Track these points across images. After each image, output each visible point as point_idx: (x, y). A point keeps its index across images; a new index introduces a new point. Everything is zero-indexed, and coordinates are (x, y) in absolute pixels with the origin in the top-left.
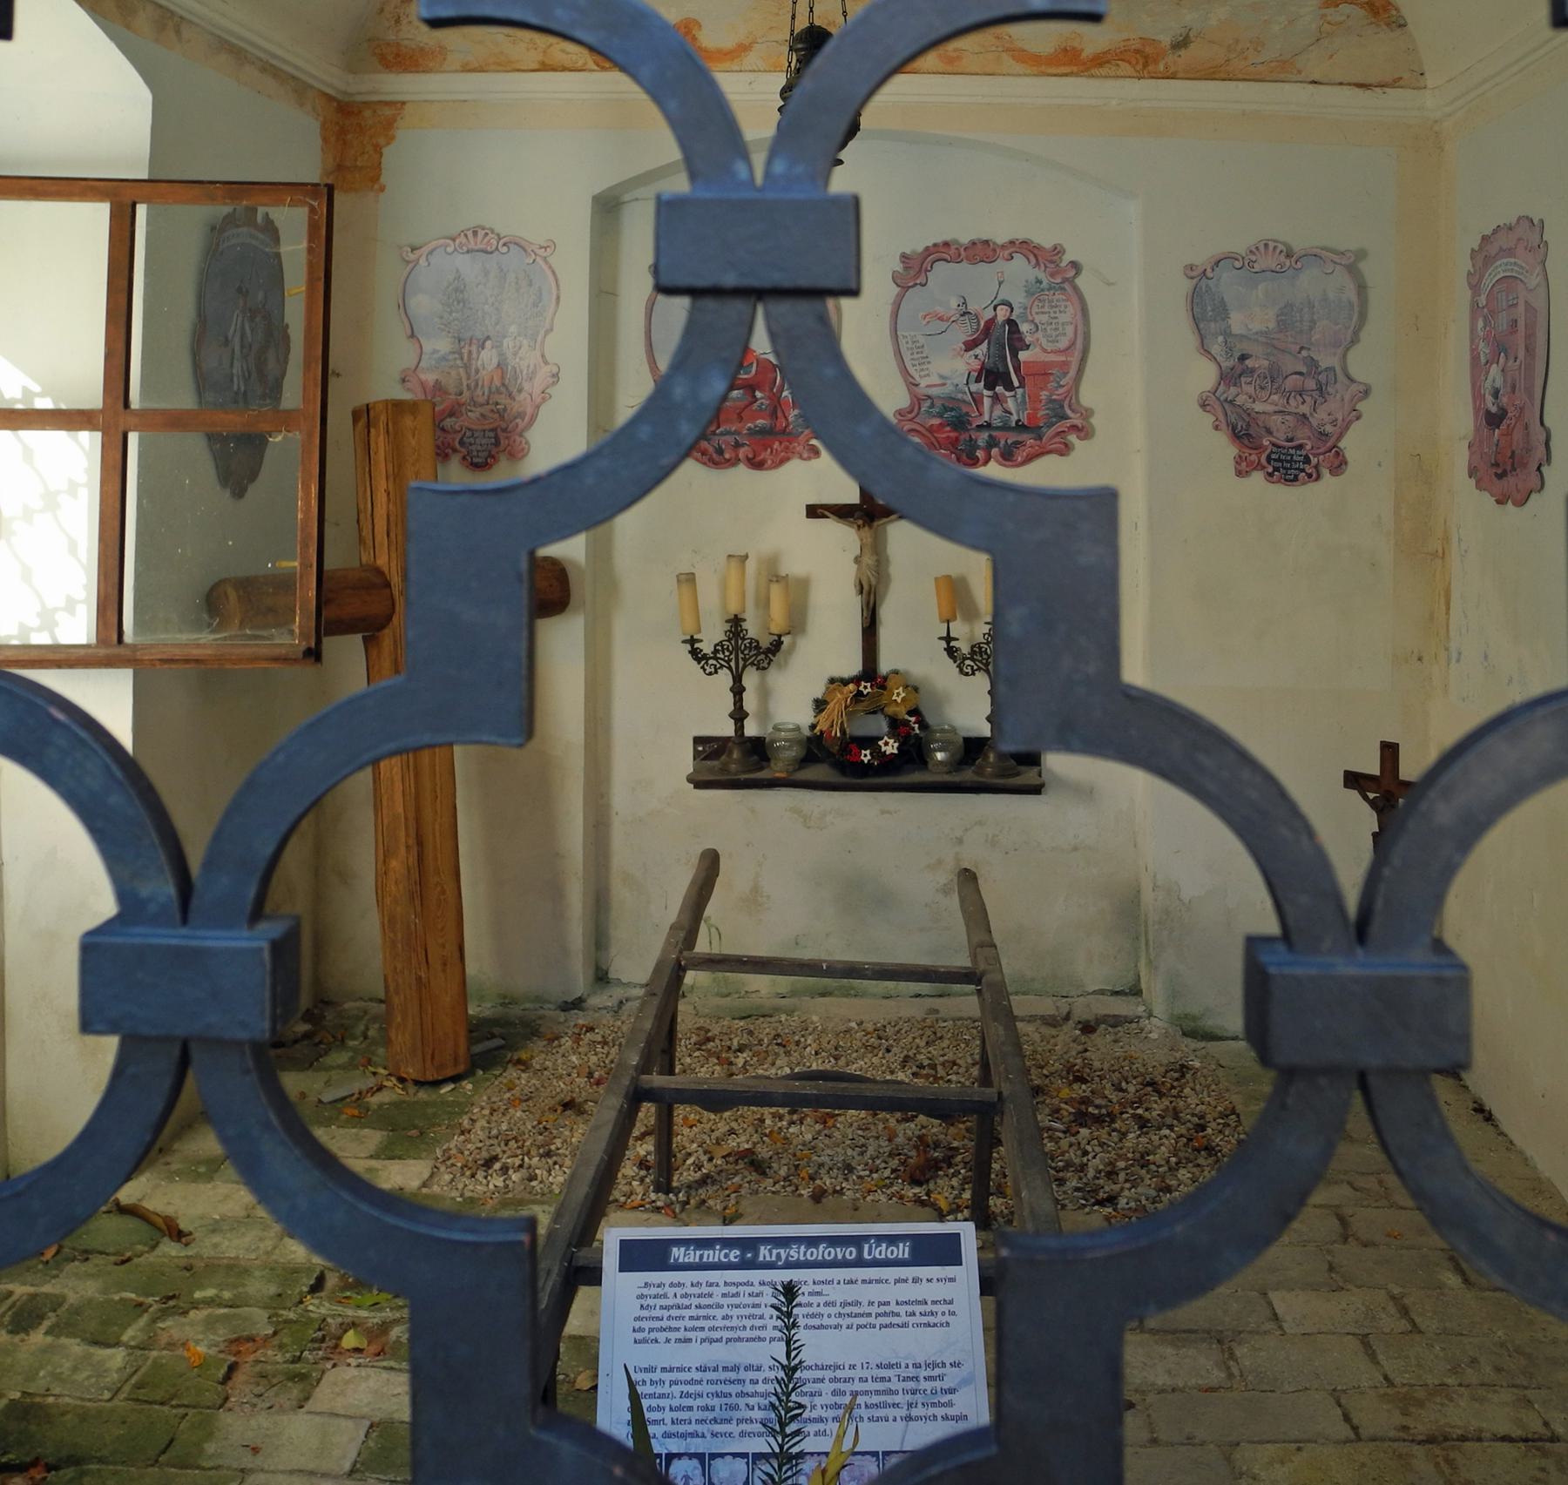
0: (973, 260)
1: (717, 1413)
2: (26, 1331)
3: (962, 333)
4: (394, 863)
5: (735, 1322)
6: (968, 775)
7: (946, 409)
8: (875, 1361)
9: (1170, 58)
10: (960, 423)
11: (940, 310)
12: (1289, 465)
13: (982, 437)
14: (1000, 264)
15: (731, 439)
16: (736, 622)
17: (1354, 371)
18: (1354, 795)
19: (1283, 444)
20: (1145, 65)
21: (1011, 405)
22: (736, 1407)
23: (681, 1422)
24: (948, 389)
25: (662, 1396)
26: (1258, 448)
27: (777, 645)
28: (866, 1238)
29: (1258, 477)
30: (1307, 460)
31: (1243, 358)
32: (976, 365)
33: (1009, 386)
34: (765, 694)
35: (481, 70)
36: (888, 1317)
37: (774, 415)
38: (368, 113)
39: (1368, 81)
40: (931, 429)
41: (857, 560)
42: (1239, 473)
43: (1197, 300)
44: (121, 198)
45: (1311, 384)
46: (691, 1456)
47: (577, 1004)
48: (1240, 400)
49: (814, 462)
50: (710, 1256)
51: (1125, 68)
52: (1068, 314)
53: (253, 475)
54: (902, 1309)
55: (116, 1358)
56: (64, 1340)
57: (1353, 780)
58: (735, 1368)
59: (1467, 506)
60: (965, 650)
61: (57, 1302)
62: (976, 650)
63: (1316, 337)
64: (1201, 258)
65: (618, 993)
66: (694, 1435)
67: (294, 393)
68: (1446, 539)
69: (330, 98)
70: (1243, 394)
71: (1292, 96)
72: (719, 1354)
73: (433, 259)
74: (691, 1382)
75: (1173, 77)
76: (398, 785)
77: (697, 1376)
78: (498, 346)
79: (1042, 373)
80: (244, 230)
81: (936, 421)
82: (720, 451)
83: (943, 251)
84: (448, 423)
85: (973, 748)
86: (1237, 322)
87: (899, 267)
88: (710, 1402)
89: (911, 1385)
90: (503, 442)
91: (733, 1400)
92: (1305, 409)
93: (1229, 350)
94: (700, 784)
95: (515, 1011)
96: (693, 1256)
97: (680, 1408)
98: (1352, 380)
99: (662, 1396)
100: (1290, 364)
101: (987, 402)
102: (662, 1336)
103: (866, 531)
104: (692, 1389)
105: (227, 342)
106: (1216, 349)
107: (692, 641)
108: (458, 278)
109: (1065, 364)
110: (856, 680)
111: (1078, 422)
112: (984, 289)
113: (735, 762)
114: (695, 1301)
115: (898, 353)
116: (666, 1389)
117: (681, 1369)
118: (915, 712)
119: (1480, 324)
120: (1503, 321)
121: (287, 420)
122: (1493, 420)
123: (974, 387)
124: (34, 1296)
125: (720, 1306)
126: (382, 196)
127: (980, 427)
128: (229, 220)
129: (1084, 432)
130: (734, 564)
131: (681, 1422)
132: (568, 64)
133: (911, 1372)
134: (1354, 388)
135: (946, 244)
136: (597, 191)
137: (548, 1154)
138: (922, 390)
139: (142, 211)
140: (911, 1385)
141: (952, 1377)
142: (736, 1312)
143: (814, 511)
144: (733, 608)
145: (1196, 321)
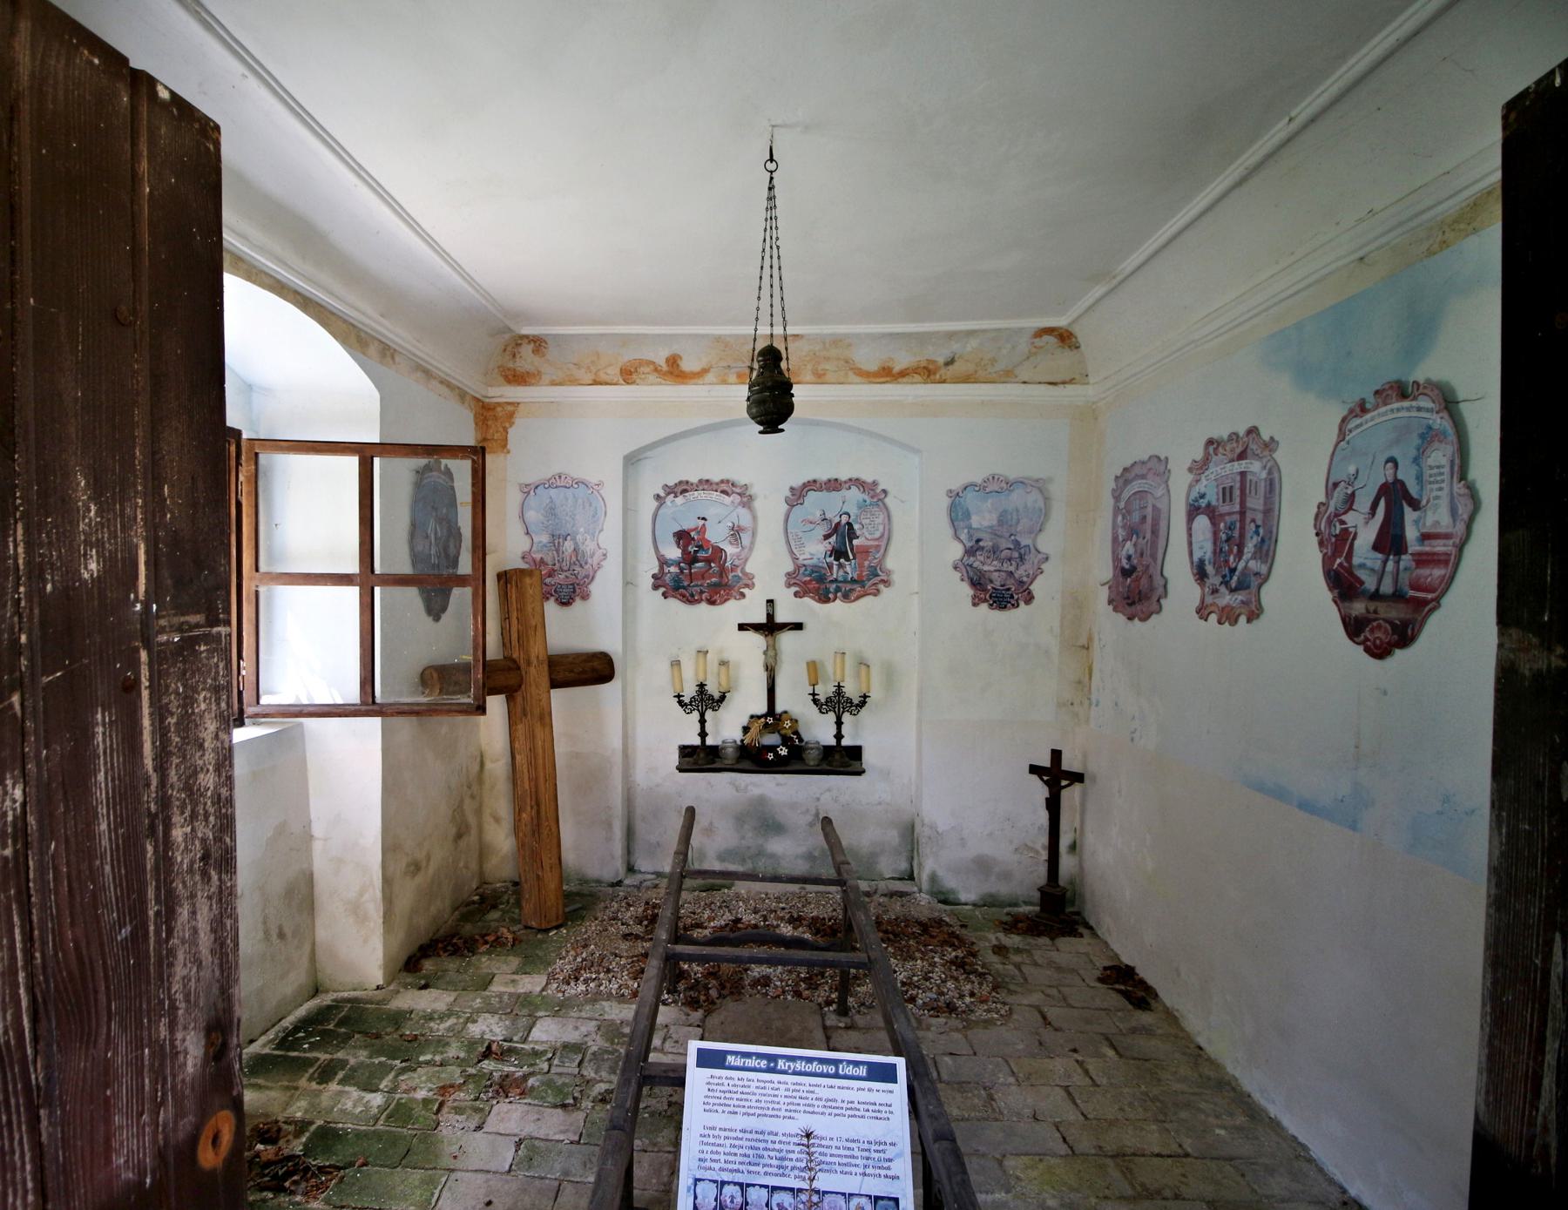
0: (828, 490)
3: (822, 530)
8: (845, 1137)
10: (821, 579)
11: (811, 518)
12: (1002, 599)
13: (833, 587)
14: (844, 492)
16: (702, 686)
17: (1040, 547)
19: (998, 585)
21: (848, 569)
22: (761, 1157)
24: (814, 561)
26: (985, 590)
27: (723, 698)
28: (841, 1061)
31: (978, 541)
33: (848, 559)
34: (717, 724)
36: (852, 1111)
37: (721, 576)
41: (765, 653)
42: (974, 605)
43: (952, 508)
45: (1016, 555)
46: (735, 1184)
47: (619, 883)
50: (750, 1063)
53: (444, 609)
54: (861, 1107)
58: (762, 1133)
59: (1108, 623)
62: (829, 700)
64: (956, 485)
65: (639, 877)
66: (737, 1171)
68: (1090, 639)
79: (865, 551)
83: (812, 485)
84: (548, 580)
86: (975, 521)
87: (788, 494)
89: (866, 1154)
91: (761, 1152)
92: (1012, 569)
93: (970, 537)
94: (681, 770)
95: (585, 889)
96: (739, 1062)
100: (1004, 544)
102: (720, 1109)
106: (963, 537)
107: (679, 696)
109: (878, 547)
110: (765, 716)
112: (834, 506)
113: (699, 758)
115: (788, 542)
118: (796, 733)
120: (1136, 517)
121: (462, 581)
122: (1126, 573)
129: (886, 583)
133: (866, 1146)
137: (608, 971)
138: (800, 562)
140: (866, 1154)
141: (891, 1152)
145: (952, 521)
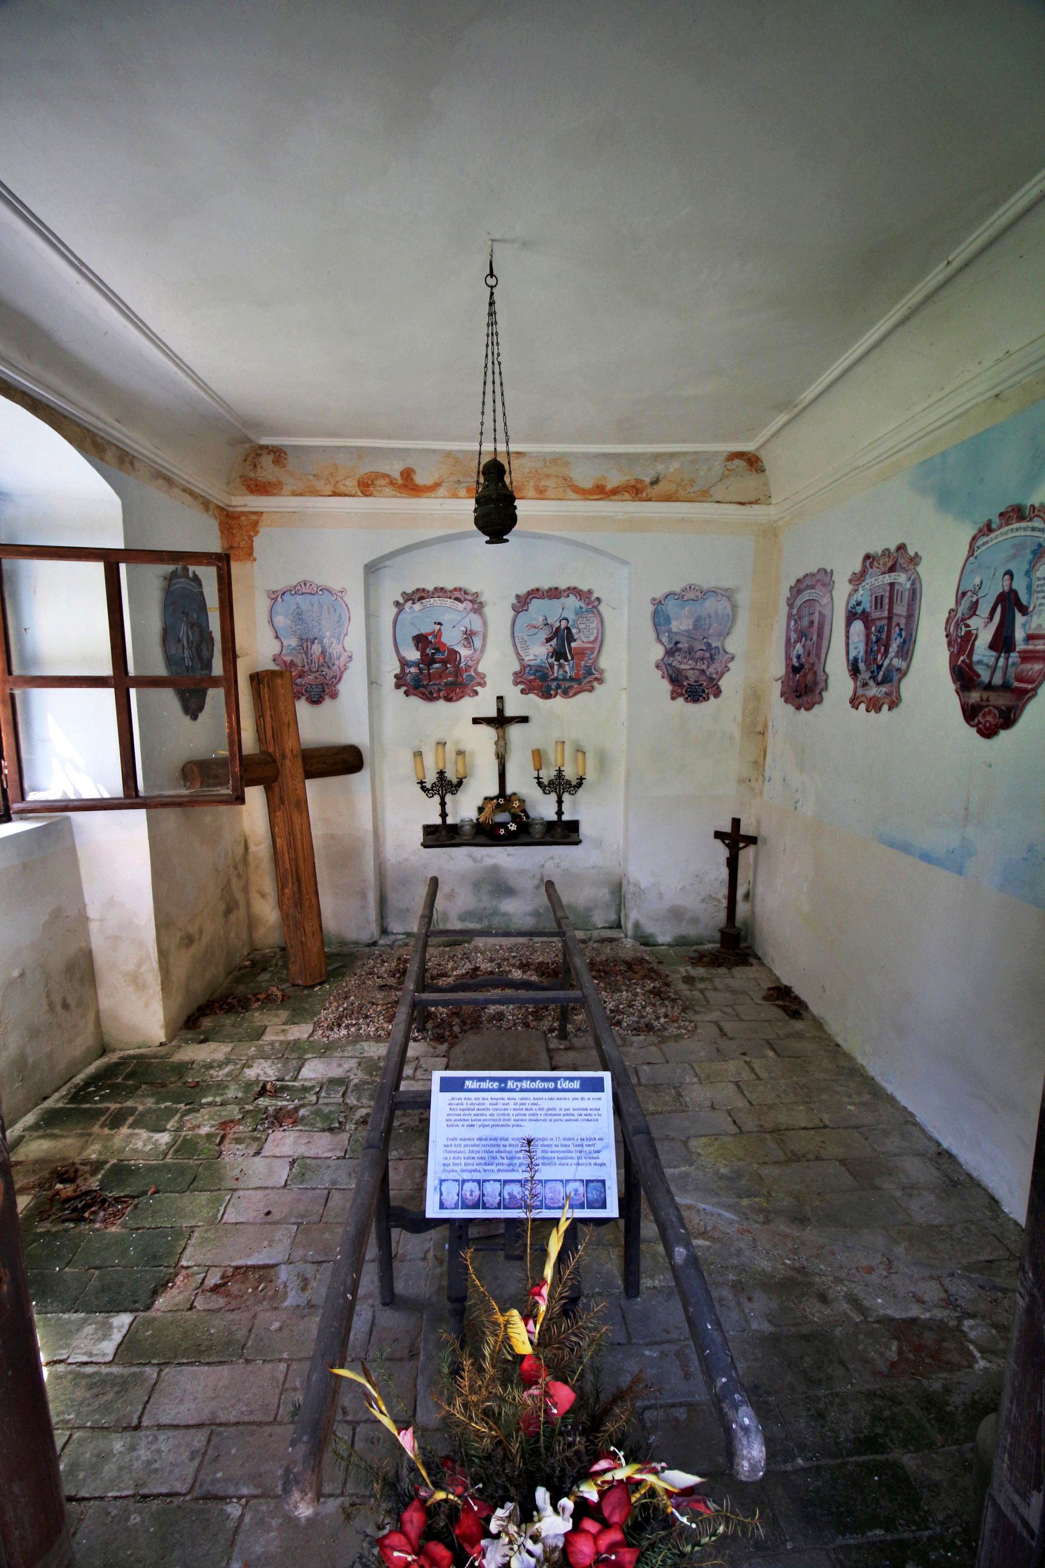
0: (550, 598)
1: (486, 1161)
2: (118, 1127)
3: (543, 635)
4: (287, 891)
5: (496, 1117)
6: (548, 839)
7: (537, 671)
9: (649, 490)
11: (535, 623)
13: (554, 685)
14: (563, 600)
15: (436, 688)
16: (441, 773)
17: (728, 649)
18: (718, 842)
20: (637, 494)
21: (567, 668)
22: (495, 1158)
23: (469, 1164)
24: (538, 662)
25: (460, 1152)
26: (681, 686)
29: (681, 700)
30: (704, 691)
31: (677, 643)
32: (551, 650)
33: (567, 660)
35: (301, 495)
37: (456, 676)
38: (243, 518)
39: (743, 501)
40: (530, 681)
43: (656, 614)
44: (110, 559)
45: (707, 655)
46: (473, 1181)
48: (674, 664)
49: (476, 698)
50: (484, 1085)
51: (626, 496)
52: (594, 624)
53: (201, 708)
55: (164, 1138)
56: (137, 1131)
57: (718, 835)
58: (495, 1139)
60: (546, 783)
61: (133, 1110)
62: (551, 782)
63: (711, 632)
64: (659, 594)
65: (392, 938)
67: (218, 668)
68: (766, 726)
69: (222, 509)
70: (676, 661)
71: (706, 509)
72: (487, 1132)
73: (285, 597)
74: (474, 1145)
75: (650, 500)
76: (286, 855)
77: (477, 1142)
78: (321, 643)
79: (582, 653)
80: (183, 580)
81: (532, 677)
82: (431, 693)
83: (535, 593)
85: (550, 825)
86: (675, 626)
87: (514, 601)
88: (483, 1155)
90: (327, 690)
91: (494, 1155)
92: (704, 667)
93: (670, 639)
95: (345, 950)
97: (469, 1158)
98: (726, 652)
99: (460, 1152)
100: (699, 646)
101: (556, 667)
103: (500, 730)
104: (475, 1149)
105: (179, 640)
107: (421, 783)
108: (298, 607)
109: (593, 648)
110: (497, 798)
111: (598, 676)
112: (554, 612)
113: (440, 835)
114: (476, 1107)
116: (462, 1149)
117: (469, 1139)
119: (793, 623)
120: (805, 622)
121: (215, 682)
123: (550, 660)
124: (121, 1109)
125: (488, 1109)
126: (255, 564)
127: (553, 680)
128: (174, 574)
129: (600, 681)
130: (440, 747)
131: (469, 1164)
132: (347, 492)
134: (727, 656)
135: (538, 590)
136: (366, 561)
138: (526, 662)
139: (123, 567)
142: (496, 1112)
143: (476, 721)
144: (441, 767)
